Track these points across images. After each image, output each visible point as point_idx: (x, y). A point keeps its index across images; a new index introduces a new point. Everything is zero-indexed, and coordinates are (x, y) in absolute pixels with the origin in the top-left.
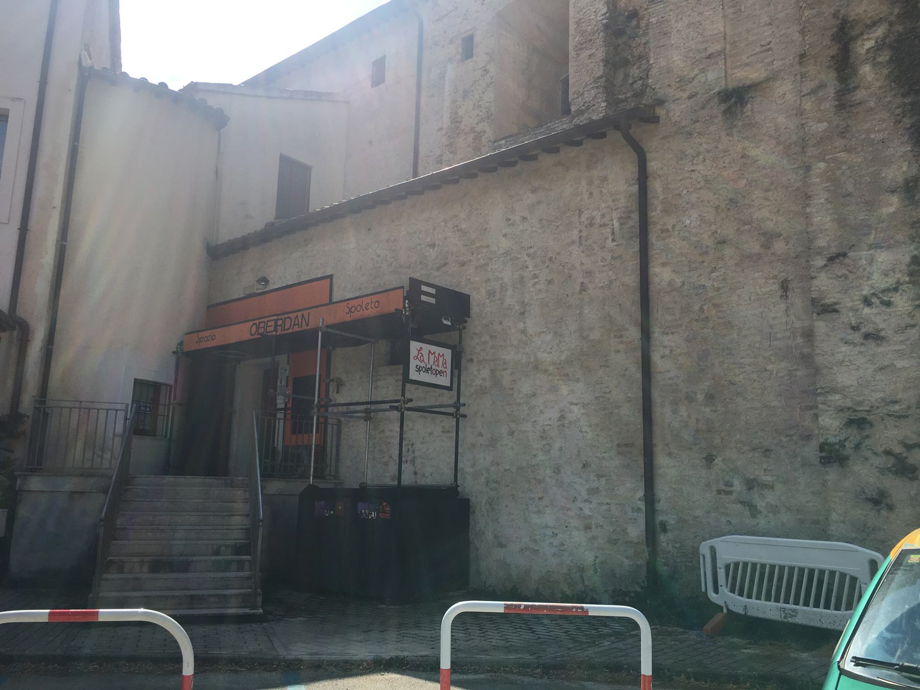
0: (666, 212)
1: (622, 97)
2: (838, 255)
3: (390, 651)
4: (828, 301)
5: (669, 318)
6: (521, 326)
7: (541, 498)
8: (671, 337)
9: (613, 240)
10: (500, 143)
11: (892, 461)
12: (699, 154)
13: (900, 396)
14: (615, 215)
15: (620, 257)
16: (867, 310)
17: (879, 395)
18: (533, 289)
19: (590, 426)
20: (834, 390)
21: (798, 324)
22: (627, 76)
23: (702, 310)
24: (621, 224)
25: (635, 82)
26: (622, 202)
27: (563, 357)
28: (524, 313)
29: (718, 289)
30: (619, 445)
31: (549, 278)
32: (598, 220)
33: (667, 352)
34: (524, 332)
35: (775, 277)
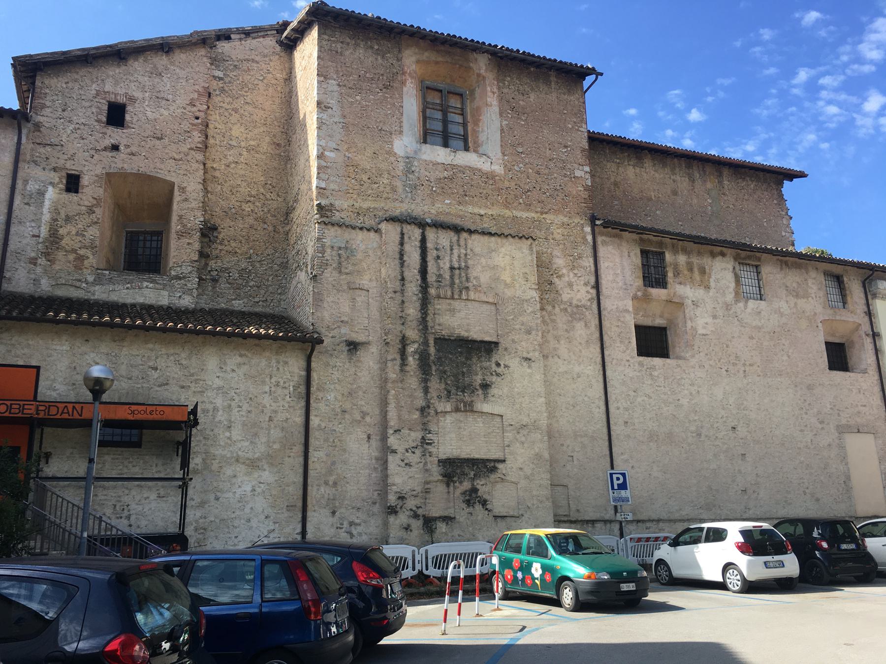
0: (318, 389)
1: (204, 277)
2: (398, 430)
4: (393, 448)
5: (318, 443)
6: (227, 434)
7: (236, 537)
10: (104, 272)
11: (412, 513)
12: (336, 366)
13: (416, 488)
14: (292, 384)
15: (293, 407)
16: (407, 454)
17: (409, 487)
18: (237, 414)
20: (394, 485)
21: (373, 454)
23: (334, 441)
26: (296, 379)
27: (256, 456)
28: (230, 427)
29: (342, 433)
30: (287, 506)
31: (249, 409)
33: (316, 460)
34: (230, 438)
35: (365, 432)
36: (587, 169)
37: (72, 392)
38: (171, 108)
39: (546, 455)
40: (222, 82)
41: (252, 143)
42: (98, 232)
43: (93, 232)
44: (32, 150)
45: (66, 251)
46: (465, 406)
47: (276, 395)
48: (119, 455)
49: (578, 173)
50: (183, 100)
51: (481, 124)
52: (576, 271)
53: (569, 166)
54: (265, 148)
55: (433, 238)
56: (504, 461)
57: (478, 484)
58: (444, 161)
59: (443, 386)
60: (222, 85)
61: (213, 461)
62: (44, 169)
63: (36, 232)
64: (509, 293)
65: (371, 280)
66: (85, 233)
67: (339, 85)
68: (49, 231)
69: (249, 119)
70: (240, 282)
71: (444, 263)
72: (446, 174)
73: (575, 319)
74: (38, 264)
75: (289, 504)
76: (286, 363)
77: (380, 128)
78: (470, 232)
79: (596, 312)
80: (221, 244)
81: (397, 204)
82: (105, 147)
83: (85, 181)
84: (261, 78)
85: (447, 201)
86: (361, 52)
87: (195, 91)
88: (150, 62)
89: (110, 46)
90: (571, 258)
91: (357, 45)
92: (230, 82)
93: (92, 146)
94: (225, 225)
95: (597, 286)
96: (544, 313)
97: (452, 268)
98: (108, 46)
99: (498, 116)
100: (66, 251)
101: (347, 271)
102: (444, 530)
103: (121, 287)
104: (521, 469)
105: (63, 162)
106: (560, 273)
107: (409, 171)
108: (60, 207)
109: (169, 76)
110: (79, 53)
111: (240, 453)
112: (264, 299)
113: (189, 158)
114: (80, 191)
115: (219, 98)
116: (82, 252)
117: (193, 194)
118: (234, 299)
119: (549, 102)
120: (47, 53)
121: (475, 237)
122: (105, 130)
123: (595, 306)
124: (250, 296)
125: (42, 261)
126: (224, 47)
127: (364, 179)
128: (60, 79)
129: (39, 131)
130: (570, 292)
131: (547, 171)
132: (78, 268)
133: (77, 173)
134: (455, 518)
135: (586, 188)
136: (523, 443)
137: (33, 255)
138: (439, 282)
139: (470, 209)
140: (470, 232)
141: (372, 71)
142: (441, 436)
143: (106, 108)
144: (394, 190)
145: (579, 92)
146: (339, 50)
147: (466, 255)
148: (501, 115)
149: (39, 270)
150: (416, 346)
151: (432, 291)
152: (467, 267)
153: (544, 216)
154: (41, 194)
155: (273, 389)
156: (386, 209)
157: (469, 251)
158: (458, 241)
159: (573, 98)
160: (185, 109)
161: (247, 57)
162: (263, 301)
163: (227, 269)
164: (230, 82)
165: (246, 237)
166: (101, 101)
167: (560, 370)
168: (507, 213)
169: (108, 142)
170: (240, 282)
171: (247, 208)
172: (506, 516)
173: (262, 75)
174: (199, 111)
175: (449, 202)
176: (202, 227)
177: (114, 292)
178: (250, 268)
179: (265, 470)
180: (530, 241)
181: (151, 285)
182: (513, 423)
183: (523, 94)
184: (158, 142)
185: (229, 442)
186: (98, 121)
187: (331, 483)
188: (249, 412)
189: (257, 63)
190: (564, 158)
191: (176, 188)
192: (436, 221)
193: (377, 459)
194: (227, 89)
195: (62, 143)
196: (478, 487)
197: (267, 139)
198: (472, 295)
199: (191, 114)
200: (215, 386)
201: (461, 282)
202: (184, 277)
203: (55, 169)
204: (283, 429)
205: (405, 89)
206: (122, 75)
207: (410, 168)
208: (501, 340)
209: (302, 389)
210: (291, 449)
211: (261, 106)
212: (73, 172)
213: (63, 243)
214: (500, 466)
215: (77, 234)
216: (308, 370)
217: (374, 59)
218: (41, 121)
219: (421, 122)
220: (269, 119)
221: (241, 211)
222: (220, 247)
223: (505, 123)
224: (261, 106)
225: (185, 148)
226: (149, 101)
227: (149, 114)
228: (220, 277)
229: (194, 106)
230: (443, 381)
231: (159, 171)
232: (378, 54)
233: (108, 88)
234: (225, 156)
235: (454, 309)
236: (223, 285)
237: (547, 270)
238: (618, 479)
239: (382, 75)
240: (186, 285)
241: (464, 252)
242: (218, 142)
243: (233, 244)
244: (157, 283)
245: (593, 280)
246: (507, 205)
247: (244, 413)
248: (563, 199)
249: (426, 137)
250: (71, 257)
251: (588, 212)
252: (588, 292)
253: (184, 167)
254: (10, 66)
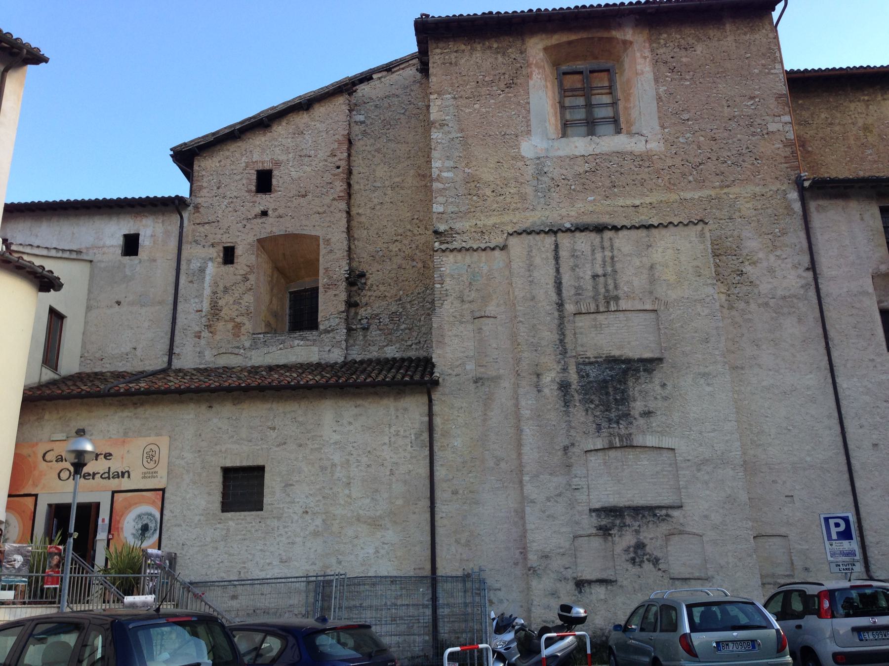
1: (354, 327)
3: (486, 663)
8: (446, 507)
9: (412, 447)
10: (259, 336)
15: (415, 457)
16: (548, 504)
19: (396, 558)
22: (356, 314)
24: (416, 438)
25: (362, 319)
26: (417, 426)
27: (378, 514)
30: (414, 569)
31: (369, 463)
32: (402, 433)
34: (349, 496)
36: (787, 118)
37: (198, 459)
38: (314, 163)
39: (743, 496)
40: (363, 125)
41: (397, 180)
42: (252, 298)
43: (249, 298)
44: (193, 231)
45: (226, 321)
46: (621, 440)
47: (396, 445)
48: (243, 520)
49: (772, 127)
50: (322, 154)
51: (632, 99)
52: (778, 253)
53: (760, 122)
54: (410, 182)
55: (568, 245)
56: (680, 507)
57: (645, 538)
58: (583, 153)
59: (591, 418)
60: (364, 129)
61: (333, 522)
62: (204, 247)
63: (199, 308)
64: (673, 295)
65: (498, 305)
66: (241, 301)
67: (455, 98)
68: (210, 304)
69: (392, 156)
70: (391, 326)
71: (584, 272)
72: (587, 167)
73: (783, 314)
74: (202, 337)
75: (417, 567)
76: (406, 409)
77: (503, 133)
78: (615, 228)
79: (815, 301)
80: (369, 290)
81: (527, 214)
82: (256, 215)
83: (238, 251)
84: (403, 111)
85: (590, 198)
86: (478, 55)
87: (336, 141)
88: (293, 123)
89: (253, 117)
90: (770, 236)
91: (473, 49)
92: (371, 124)
93: (244, 216)
94: (373, 270)
95: (813, 267)
96: (734, 313)
97: (595, 277)
98: (251, 118)
99: (653, 83)
100: (226, 321)
101: (470, 299)
102: (602, 597)
103: (274, 349)
104: (706, 517)
105: (220, 236)
106: (755, 258)
107: (540, 173)
108: (218, 279)
109: (310, 132)
110: (227, 131)
111: (361, 512)
112: (417, 341)
113: (332, 209)
114: (235, 261)
115: (361, 142)
116: (238, 320)
117: (337, 244)
118: (387, 346)
119: (724, 49)
120: (199, 138)
121: (622, 233)
122: (255, 199)
123: (812, 293)
124: (402, 340)
125: (205, 334)
126: (364, 90)
127: (487, 194)
128: (214, 159)
129: (199, 212)
130: (771, 280)
131: (726, 134)
132: (236, 335)
133: (232, 245)
134: (616, 581)
135: (788, 144)
136: (706, 483)
137: (197, 329)
138: (579, 294)
139: (621, 202)
140: (615, 228)
141: (492, 72)
142: (592, 480)
143: (255, 177)
144: (523, 198)
145: (768, 27)
146: (454, 61)
147: (612, 258)
148: (656, 80)
149: (203, 342)
150: (553, 374)
151: (570, 308)
152: (615, 271)
153: (726, 190)
154: (202, 270)
155: (393, 439)
156: (515, 221)
157: (615, 252)
158: (602, 242)
159: (760, 36)
160: (326, 161)
161: (387, 94)
162: (416, 344)
163: (377, 315)
164: (371, 124)
165: (395, 279)
166: (251, 172)
167: (764, 383)
168: (673, 197)
169: (258, 210)
170: (391, 326)
171: (394, 248)
172: (689, 579)
173: (404, 108)
174: (340, 160)
175: (592, 198)
176: (347, 276)
177: (269, 355)
178: (401, 310)
179: (388, 529)
180: (699, 227)
181: (302, 343)
182: (690, 458)
183: (686, 49)
184: (302, 200)
185: (349, 500)
186: (249, 191)
187: (463, 541)
188: (368, 466)
189: (397, 96)
190: (750, 112)
191: (321, 242)
192: (577, 225)
193: (516, 511)
194: (369, 131)
195: (218, 219)
196: (646, 541)
197: (412, 172)
198: (623, 305)
199: (332, 165)
200: (332, 441)
201: (607, 291)
202: (333, 330)
203: (213, 245)
204: (405, 482)
205: (531, 83)
206: (267, 142)
207: (542, 170)
208: (666, 355)
209: (426, 436)
210: (416, 504)
211: (404, 140)
212: (229, 245)
213: (222, 314)
214: (675, 513)
215: (234, 302)
216: (431, 414)
217: (493, 60)
218: (200, 202)
219: (558, 114)
220: (413, 152)
221: (388, 253)
222: (369, 293)
223: (662, 89)
224: (404, 140)
225: (327, 200)
226: (293, 162)
227: (293, 174)
228: (371, 324)
229: (335, 156)
230: (590, 412)
231: (305, 228)
232: (498, 53)
233: (256, 157)
234: (370, 200)
235: (601, 324)
236: (374, 333)
237: (734, 258)
238: (837, 525)
239: (504, 74)
240: (334, 338)
241: (610, 254)
242: (362, 187)
243: (382, 288)
244: (308, 340)
245: (806, 260)
246: (670, 187)
247: (362, 468)
248: (753, 164)
249: (566, 128)
250: (230, 325)
251: (792, 173)
252: (799, 277)
253: (328, 219)
254: (171, 159)
